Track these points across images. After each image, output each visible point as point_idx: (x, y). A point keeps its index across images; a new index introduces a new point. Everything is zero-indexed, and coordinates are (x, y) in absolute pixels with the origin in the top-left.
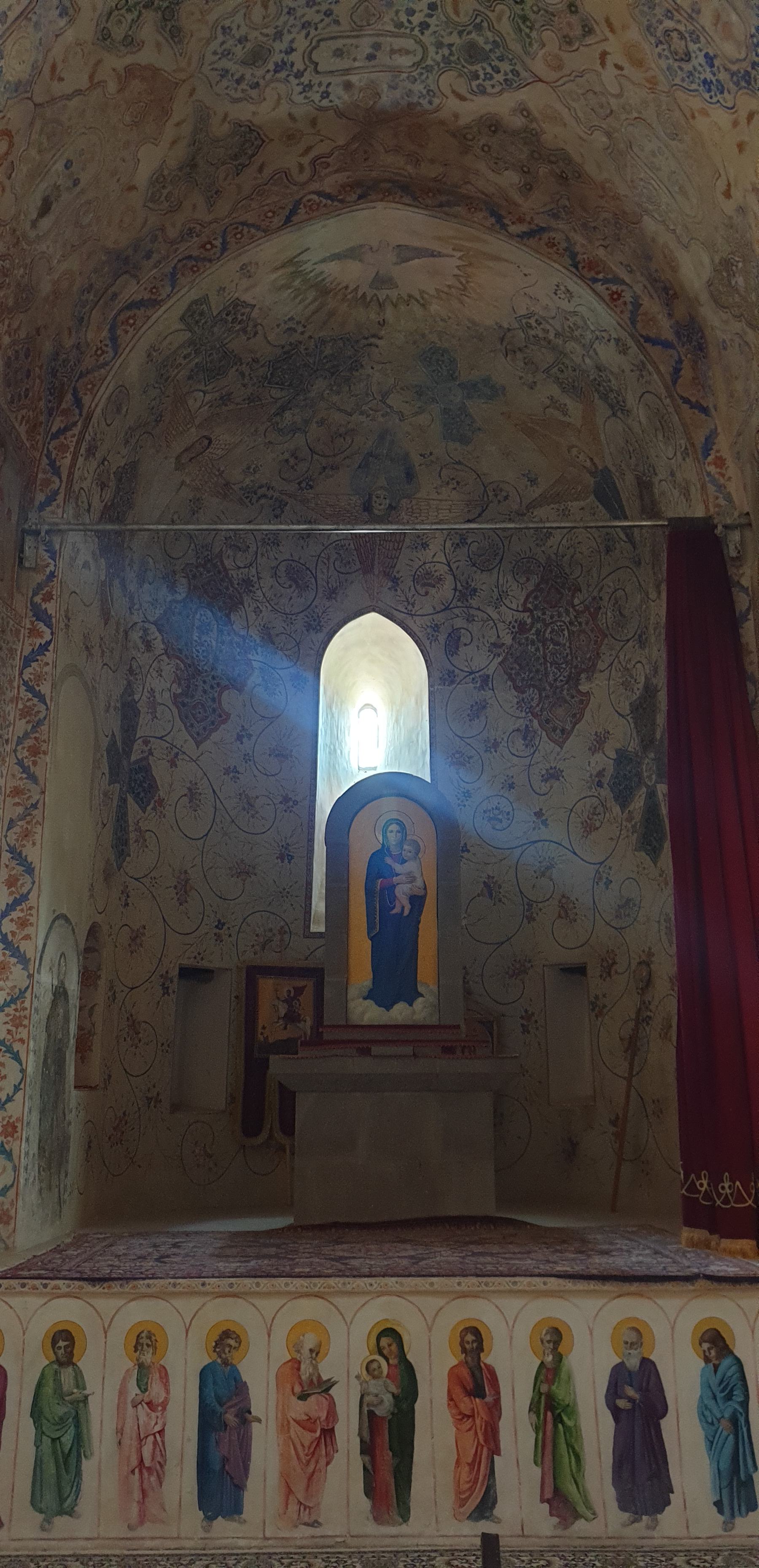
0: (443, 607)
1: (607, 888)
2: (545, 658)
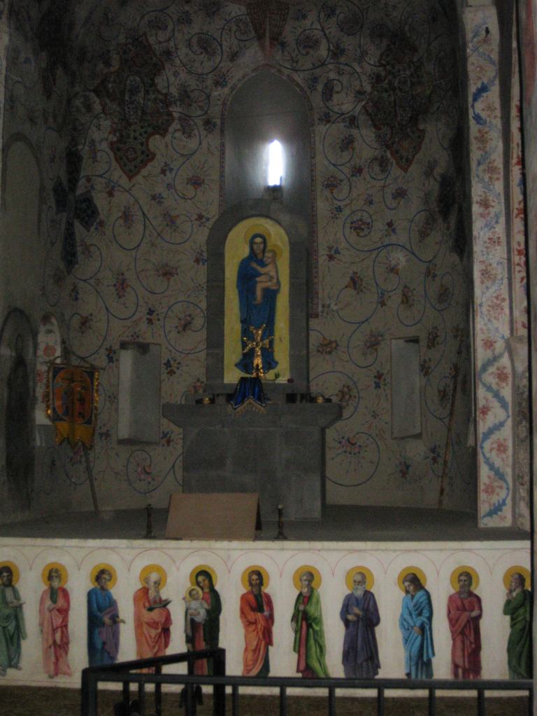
0: (320, 64)
1: (434, 280)
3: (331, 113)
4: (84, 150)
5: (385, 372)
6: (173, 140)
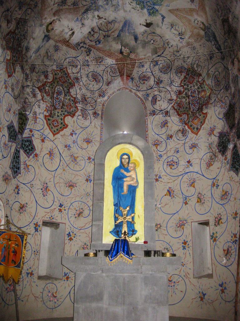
1: (217, 188)
2: (189, 102)
3: (156, 111)
4: (30, 116)
5: (189, 240)
6: (77, 120)
